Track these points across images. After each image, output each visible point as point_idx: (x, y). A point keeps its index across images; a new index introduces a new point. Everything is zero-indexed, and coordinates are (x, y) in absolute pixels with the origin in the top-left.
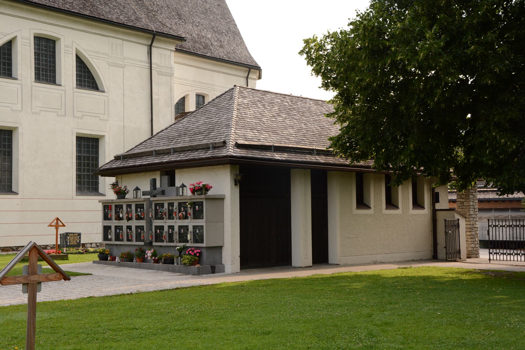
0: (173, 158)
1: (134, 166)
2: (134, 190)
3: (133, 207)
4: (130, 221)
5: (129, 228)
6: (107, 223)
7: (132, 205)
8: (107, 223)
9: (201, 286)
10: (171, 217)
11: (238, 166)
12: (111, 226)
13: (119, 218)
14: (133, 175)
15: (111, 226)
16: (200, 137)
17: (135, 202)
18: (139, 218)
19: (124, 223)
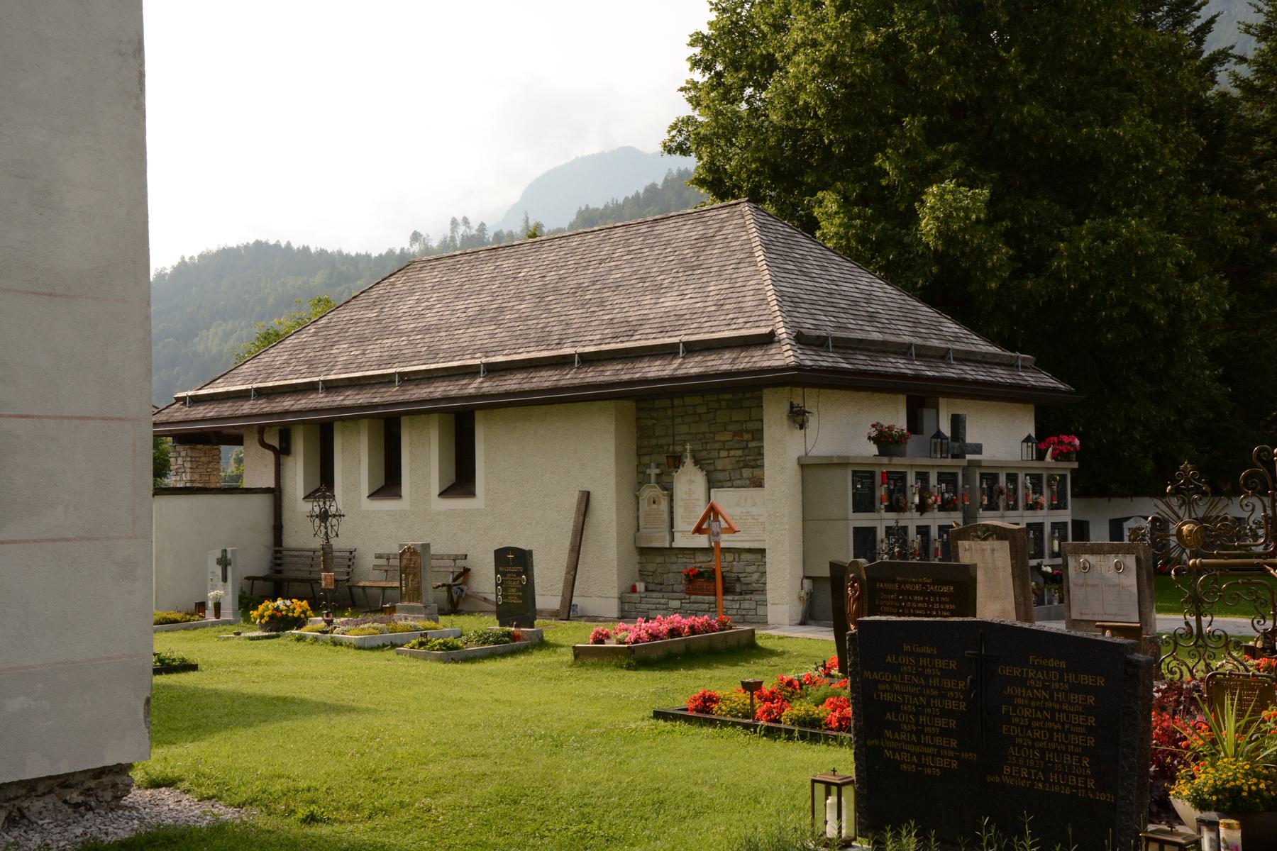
0: (474, 386)
1: (962, 381)
2: (1023, 442)
3: (933, 480)
4: (927, 515)
5: (923, 531)
6: (864, 520)
7: (931, 475)
8: (864, 520)
9: (918, 621)
10: (922, 508)
11: (364, 424)
12: (876, 527)
13: (895, 506)
14: (838, 394)
15: (876, 527)
16: (278, 362)
17: (937, 466)
18: (946, 506)
19: (911, 520)
